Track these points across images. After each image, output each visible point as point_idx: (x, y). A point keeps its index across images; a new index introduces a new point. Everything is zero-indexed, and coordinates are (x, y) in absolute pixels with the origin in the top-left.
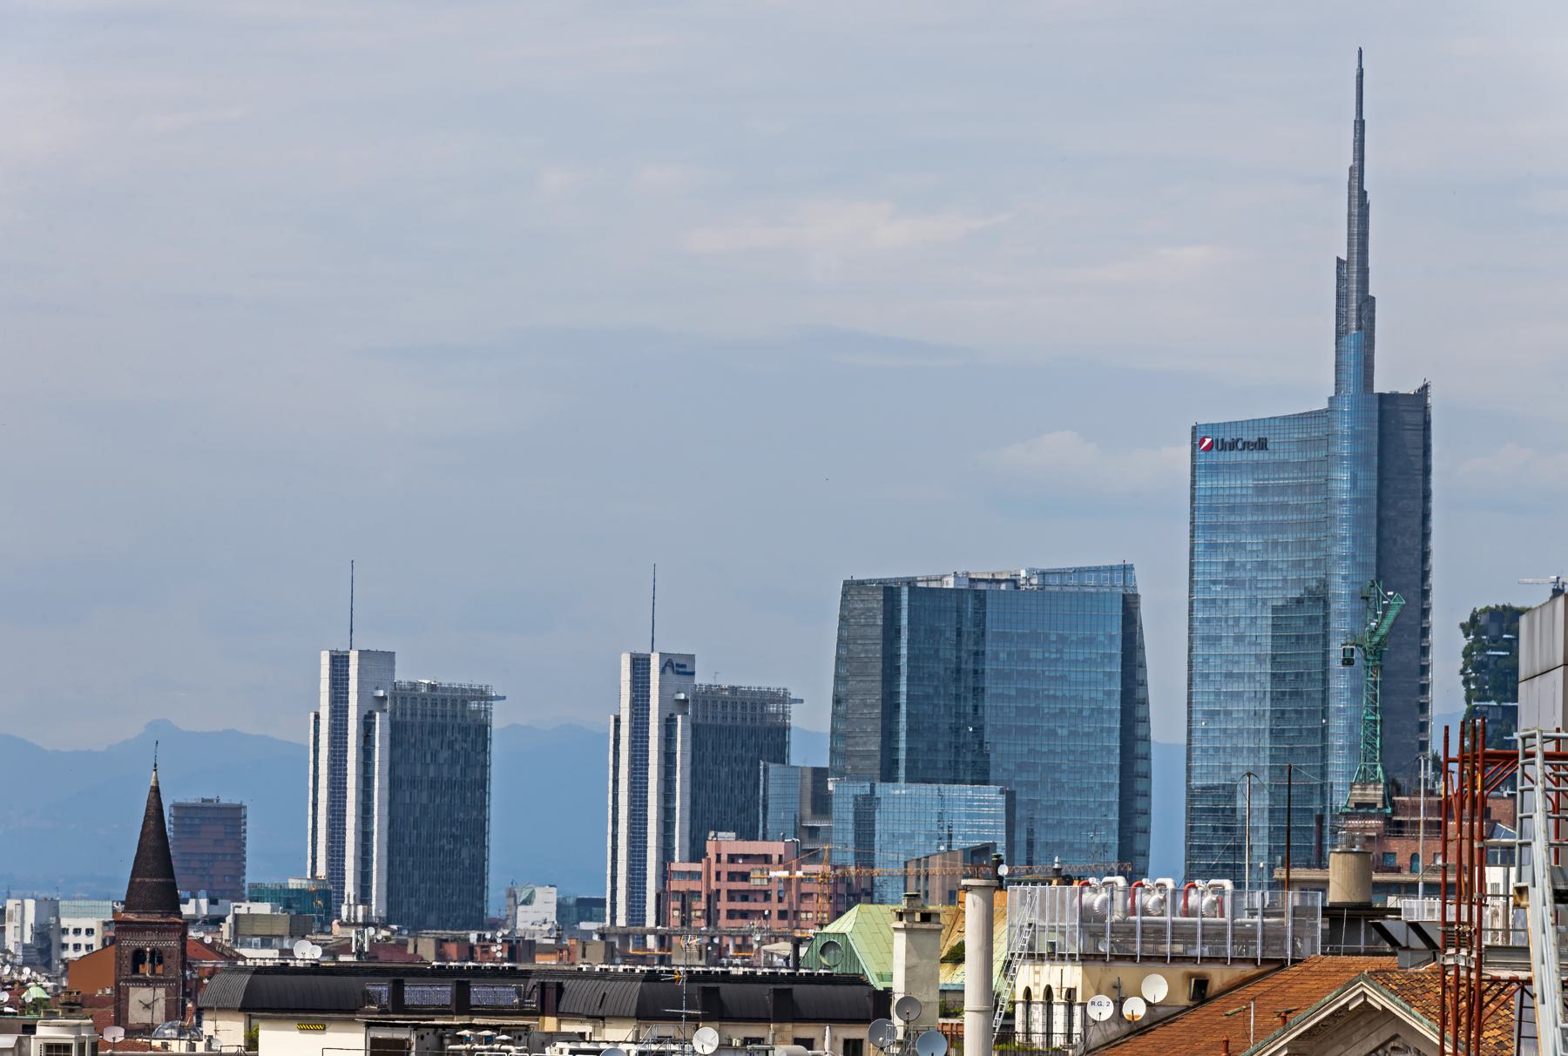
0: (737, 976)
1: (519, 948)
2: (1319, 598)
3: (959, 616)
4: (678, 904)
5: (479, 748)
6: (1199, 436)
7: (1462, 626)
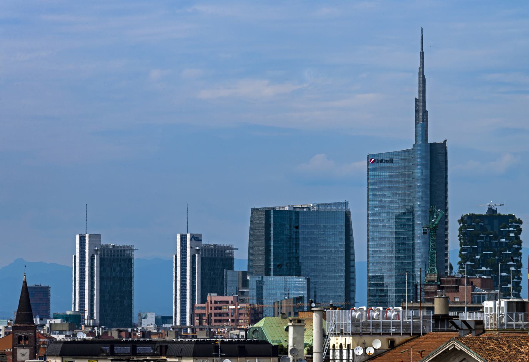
0: (226, 342)
1: (146, 333)
2: (411, 212)
3: (291, 220)
4: (198, 318)
5: (130, 267)
6: (370, 158)
7: (458, 221)
